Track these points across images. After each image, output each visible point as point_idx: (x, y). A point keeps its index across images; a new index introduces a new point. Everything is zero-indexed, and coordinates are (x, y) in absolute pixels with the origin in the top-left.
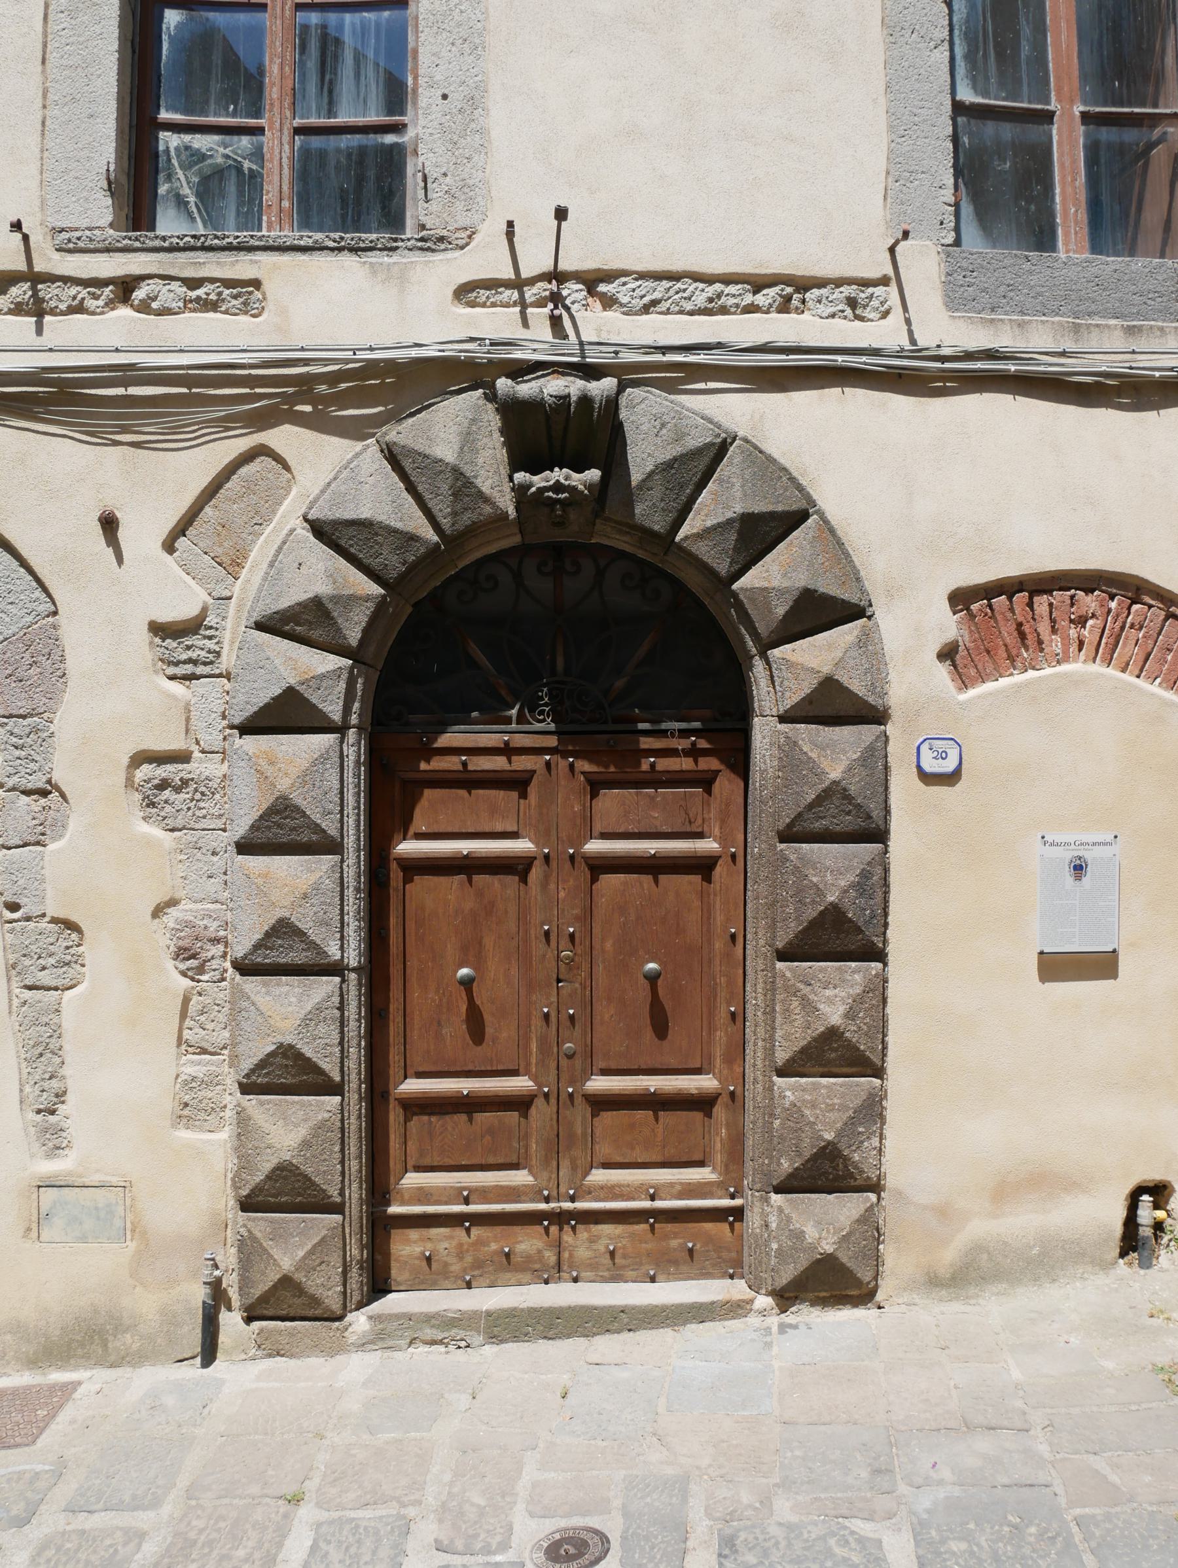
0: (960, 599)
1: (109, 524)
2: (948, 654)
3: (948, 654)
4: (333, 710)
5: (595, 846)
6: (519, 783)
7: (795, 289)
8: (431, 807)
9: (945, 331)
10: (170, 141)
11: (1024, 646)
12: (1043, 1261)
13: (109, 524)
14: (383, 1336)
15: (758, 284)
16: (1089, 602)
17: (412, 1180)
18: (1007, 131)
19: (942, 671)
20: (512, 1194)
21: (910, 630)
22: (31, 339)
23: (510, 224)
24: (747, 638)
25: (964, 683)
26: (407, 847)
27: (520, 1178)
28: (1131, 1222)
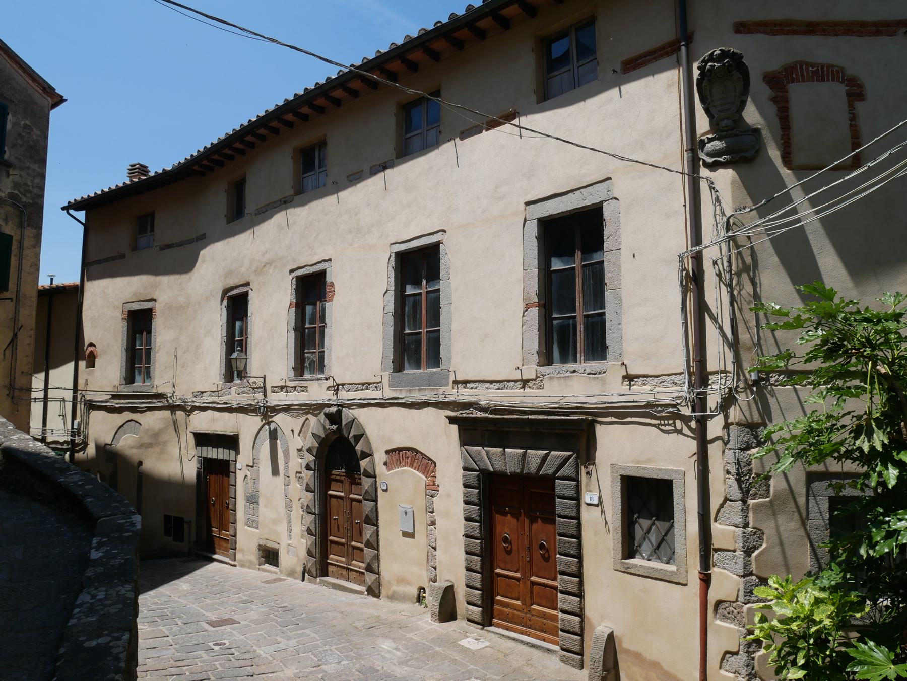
0: (387, 452)
1: (292, 431)
2: (385, 464)
3: (385, 464)
4: (313, 467)
5: (352, 496)
6: (341, 481)
7: (367, 385)
8: (334, 485)
9: (389, 393)
10: (306, 355)
11: (399, 463)
12: (403, 598)
13: (292, 431)
14: (321, 583)
15: (363, 384)
16: (408, 453)
17: (331, 556)
18: (414, 337)
19: (385, 467)
20: (342, 562)
21: (380, 457)
22: (285, 398)
23: (610, 179)
24: (530, 417)
25: (389, 470)
26: (330, 492)
27: (343, 559)
28: (419, 595)
